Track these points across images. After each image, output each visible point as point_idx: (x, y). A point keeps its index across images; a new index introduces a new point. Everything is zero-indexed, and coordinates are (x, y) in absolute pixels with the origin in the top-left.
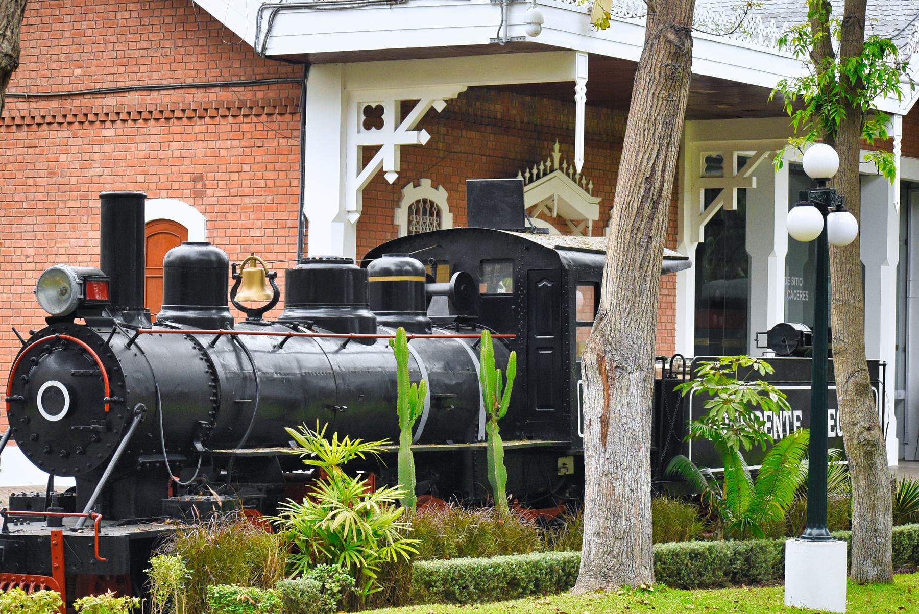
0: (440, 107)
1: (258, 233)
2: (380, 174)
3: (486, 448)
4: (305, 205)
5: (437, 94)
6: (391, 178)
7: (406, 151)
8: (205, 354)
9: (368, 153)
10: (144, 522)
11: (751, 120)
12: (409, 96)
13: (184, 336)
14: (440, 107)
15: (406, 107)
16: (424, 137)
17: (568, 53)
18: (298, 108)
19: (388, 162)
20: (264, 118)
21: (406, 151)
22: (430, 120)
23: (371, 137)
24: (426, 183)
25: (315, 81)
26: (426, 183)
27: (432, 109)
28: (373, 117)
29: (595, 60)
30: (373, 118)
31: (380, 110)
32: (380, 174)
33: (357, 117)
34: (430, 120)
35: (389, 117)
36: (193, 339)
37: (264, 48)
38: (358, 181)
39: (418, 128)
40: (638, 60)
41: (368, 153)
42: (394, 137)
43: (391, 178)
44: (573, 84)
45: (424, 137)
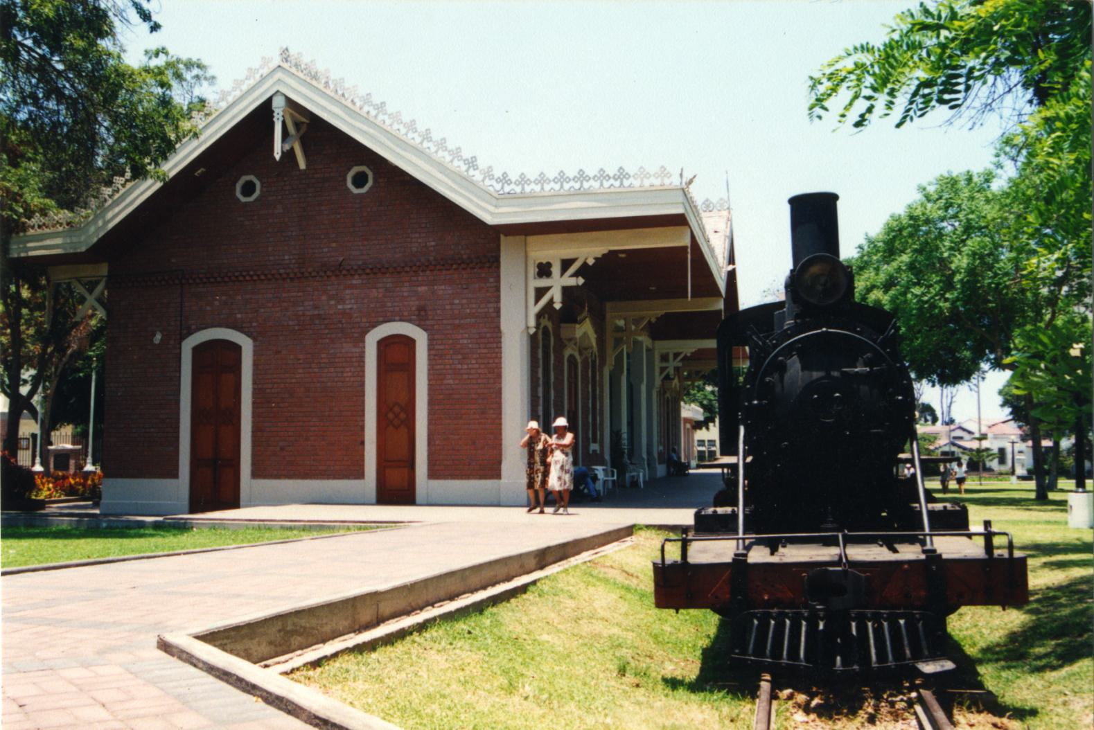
0: (591, 262)
1: (465, 341)
2: (551, 302)
3: (492, 470)
4: (187, 556)
5: (589, 250)
7: (566, 290)
10: (908, 635)
11: (366, 454)
14: (591, 262)
16: (581, 281)
18: (494, 263)
19: (556, 295)
20: (469, 270)
21: (566, 290)
23: (543, 283)
28: (544, 270)
31: (549, 265)
32: (551, 302)
34: (584, 271)
35: (556, 270)
38: (534, 310)
39: (576, 275)
40: (562, 325)
41: (540, 292)
42: (558, 283)
45: (581, 281)
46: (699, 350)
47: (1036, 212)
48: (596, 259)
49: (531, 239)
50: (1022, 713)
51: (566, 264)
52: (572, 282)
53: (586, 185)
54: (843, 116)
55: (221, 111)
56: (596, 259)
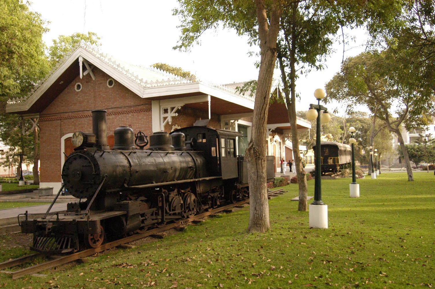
0: (180, 108)
2: (168, 122)
5: (179, 105)
6: (170, 123)
7: (173, 118)
8: (127, 158)
9: (165, 118)
12: (173, 106)
13: (149, 238)
15: (172, 109)
17: (205, 95)
18: (150, 110)
19: (170, 120)
21: (173, 118)
22: (178, 111)
23: (166, 115)
24: (176, 125)
25: (153, 102)
26: (176, 125)
27: (178, 109)
29: (212, 97)
30: (166, 111)
31: (167, 109)
32: (168, 122)
33: (162, 111)
34: (178, 111)
35: (169, 111)
36: (123, 154)
37: (9, 168)
39: (175, 113)
41: (165, 118)
42: (170, 115)
43: (170, 123)
44: (208, 102)
45: (177, 114)
46: (186, 104)
47: (390, 121)
48: (181, 107)
49: (161, 101)
50: (161, 67)
51: (172, 109)
52: (174, 115)
53: (102, 57)
54: (363, 45)
55: (321, 133)
56: (181, 107)
